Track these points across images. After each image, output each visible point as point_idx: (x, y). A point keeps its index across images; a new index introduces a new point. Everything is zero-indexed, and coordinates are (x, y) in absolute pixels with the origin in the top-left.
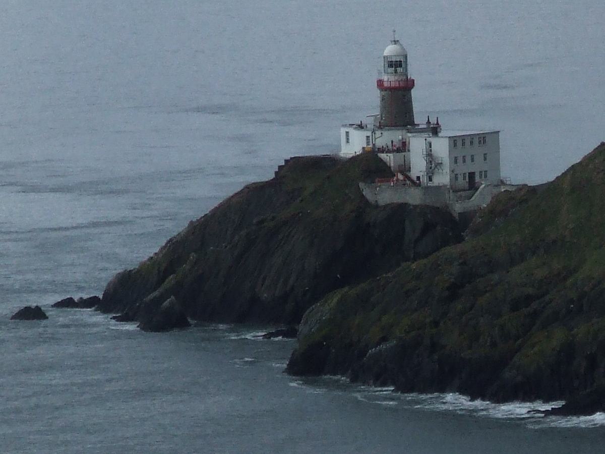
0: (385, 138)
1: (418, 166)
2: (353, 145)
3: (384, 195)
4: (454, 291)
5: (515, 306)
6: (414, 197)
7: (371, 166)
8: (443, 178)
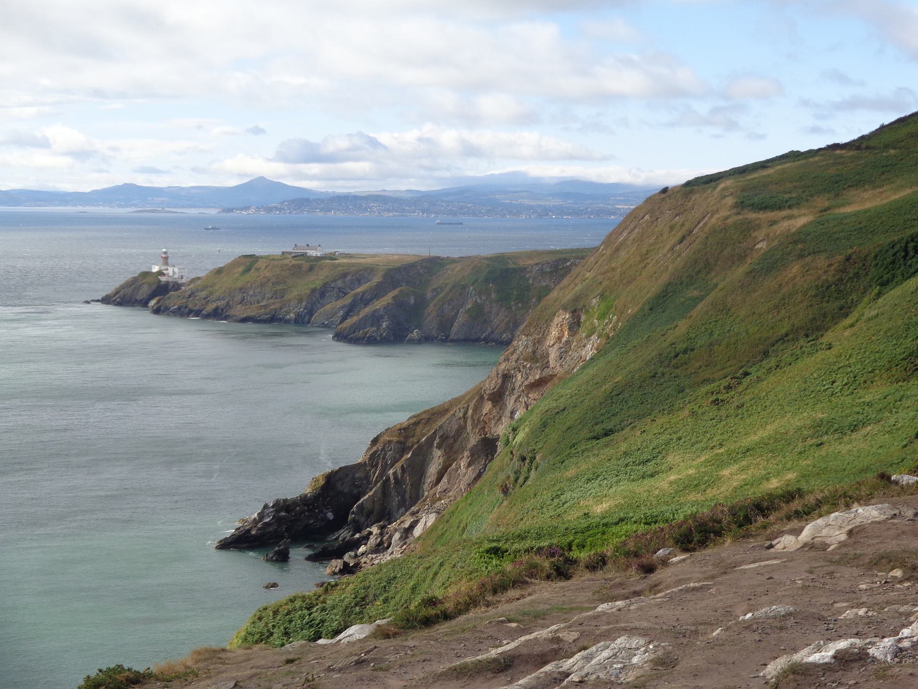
0: (163, 268)
2: (155, 269)
3: (163, 279)
4: (190, 296)
6: (170, 280)
7: (160, 273)
8: (176, 276)
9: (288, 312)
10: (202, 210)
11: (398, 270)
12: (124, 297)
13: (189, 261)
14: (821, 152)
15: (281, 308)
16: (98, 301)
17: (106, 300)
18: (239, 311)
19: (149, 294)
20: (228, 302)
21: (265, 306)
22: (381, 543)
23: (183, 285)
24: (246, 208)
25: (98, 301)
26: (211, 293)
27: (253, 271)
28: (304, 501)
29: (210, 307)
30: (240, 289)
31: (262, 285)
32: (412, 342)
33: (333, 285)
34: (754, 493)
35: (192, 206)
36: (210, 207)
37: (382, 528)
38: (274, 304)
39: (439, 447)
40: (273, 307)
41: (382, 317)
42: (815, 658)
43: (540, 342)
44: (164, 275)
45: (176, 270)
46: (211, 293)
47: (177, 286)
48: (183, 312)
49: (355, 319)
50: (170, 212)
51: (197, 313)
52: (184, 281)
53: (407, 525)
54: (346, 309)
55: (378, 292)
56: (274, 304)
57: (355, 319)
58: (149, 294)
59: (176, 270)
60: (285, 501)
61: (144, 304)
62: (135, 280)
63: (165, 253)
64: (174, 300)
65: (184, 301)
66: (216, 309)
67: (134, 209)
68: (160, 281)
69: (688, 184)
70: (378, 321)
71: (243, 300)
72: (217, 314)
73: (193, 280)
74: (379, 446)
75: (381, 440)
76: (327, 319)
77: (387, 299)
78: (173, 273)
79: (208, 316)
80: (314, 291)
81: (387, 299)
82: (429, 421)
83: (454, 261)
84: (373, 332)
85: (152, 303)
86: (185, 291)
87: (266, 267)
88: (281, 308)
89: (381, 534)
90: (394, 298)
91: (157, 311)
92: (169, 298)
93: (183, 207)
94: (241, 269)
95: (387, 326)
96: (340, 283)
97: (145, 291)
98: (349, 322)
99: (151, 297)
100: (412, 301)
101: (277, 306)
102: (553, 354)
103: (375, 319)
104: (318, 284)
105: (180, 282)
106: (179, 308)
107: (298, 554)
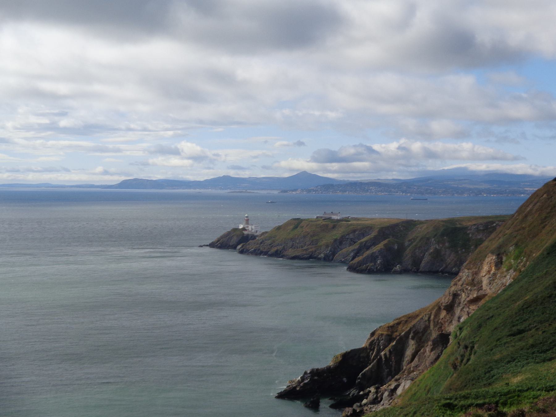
1: (250, 229)
2: (241, 227)
3: (245, 233)
4: (261, 243)
5: (270, 245)
6: (250, 233)
7: (244, 229)
8: (253, 231)
9: (320, 253)
10: (269, 191)
11: (387, 228)
12: (222, 244)
13: (261, 222)
15: (315, 251)
16: (207, 246)
17: (212, 245)
18: (291, 252)
19: (236, 242)
20: (284, 247)
21: (306, 250)
22: (377, 398)
23: (257, 236)
24: (295, 190)
25: (207, 246)
26: (274, 242)
27: (299, 228)
28: (329, 370)
29: (273, 250)
30: (291, 239)
31: (304, 237)
33: (347, 237)
35: (262, 189)
36: (274, 189)
38: (311, 248)
39: (413, 338)
40: (310, 250)
41: (377, 257)
43: (476, 273)
44: (246, 230)
45: (253, 227)
46: (274, 242)
47: (253, 237)
48: (257, 253)
50: (250, 192)
51: (266, 253)
52: (258, 234)
54: (355, 252)
56: (311, 248)
58: (236, 242)
59: (253, 227)
60: (317, 370)
61: (234, 247)
62: (229, 233)
63: (247, 217)
64: (252, 245)
65: (258, 246)
66: (277, 251)
67: (229, 191)
68: (243, 234)
70: (375, 259)
71: (293, 245)
72: (277, 254)
73: (263, 234)
74: (375, 337)
75: (377, 333)
76: (343, 258)
77: (380, 246)
78: (251, 229)
79: (272, 255)
80: (335, 240)
81: (380, 246)
83: (421, 223)
84: (372, 266)
85: (239, 247)
86: (258, 240)
87: (307, 225)
88: (315, 251)
89: (377, 392)
90: (385, 245)
91: (242, 252)
92: (249, 244)
93: (258, 189)
94: (292, 227)
95: (381, 263)
96: (351, 236)
97: (234, 240)
98: (357, 259)
99: (238, 244)
100: (396, 247)
101: (313, 249)
102: (485, 281)
103: (373, 258)
104: (338, 236)
105: (256, 234)
106: (255, 250)
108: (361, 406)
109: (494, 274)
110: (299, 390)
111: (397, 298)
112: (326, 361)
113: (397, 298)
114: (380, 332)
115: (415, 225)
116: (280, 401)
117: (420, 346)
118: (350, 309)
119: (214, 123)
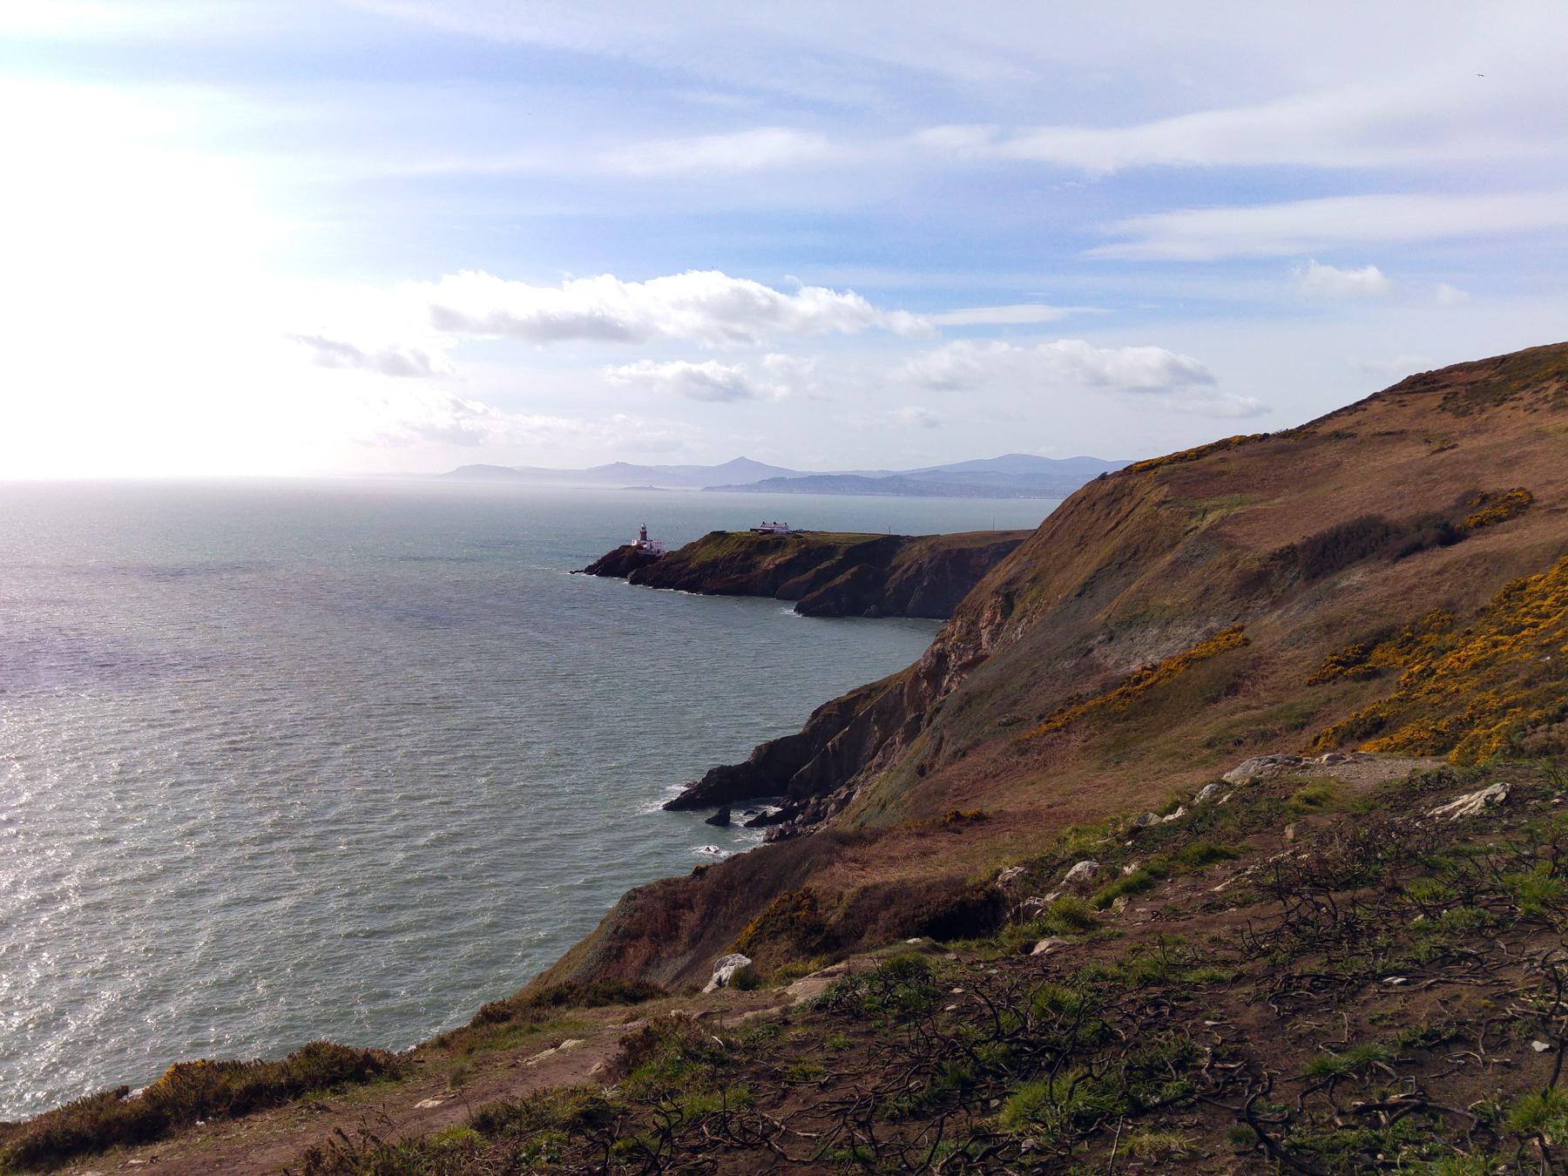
2: (635, 543)
7: (639, 547)
13: (669, 541)
14: (1248, 448)
19: (633, 564)
22: (818, 812)
32: (869, 616)
34: (1224, 868)
37: (819, 799)
39: (876, 722)
42: (1218, 889)
43: (974, 623)
49: (815, 594)
53: (842, 797)
55: (841, 567)
57: (815, 594)
69: (1130, 471)
74: (820, 718)
77: (847, 575)
81: (847, 575)
82: (868, 696)
83: (911, 540)
89: (819, 804)
98: (810, 596)
102: (985, 636)
107: (739, 818)
108: (284, 808)
109: (1000, 625)
110: (809, 797)
111: (883, 651)
112: (739, 756)
113: (883, 651)
114: (825, 711)
115: (900, 546)
116: (671, 814)
117: (887, 732)
118: (822, 662)
119: (466, 560)
